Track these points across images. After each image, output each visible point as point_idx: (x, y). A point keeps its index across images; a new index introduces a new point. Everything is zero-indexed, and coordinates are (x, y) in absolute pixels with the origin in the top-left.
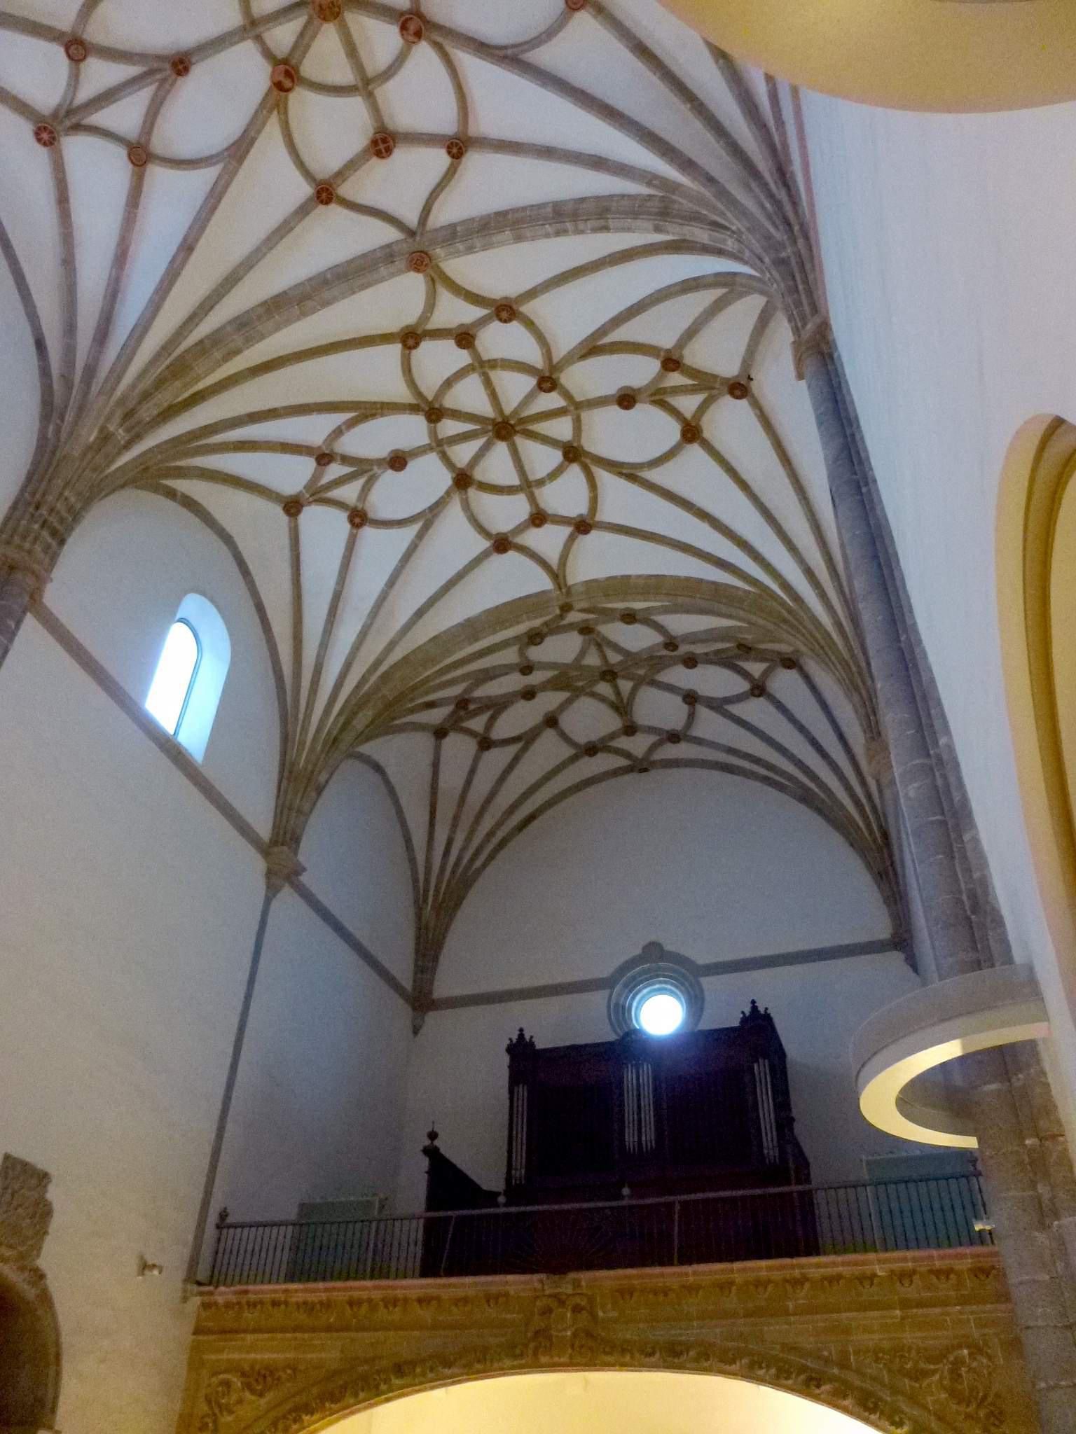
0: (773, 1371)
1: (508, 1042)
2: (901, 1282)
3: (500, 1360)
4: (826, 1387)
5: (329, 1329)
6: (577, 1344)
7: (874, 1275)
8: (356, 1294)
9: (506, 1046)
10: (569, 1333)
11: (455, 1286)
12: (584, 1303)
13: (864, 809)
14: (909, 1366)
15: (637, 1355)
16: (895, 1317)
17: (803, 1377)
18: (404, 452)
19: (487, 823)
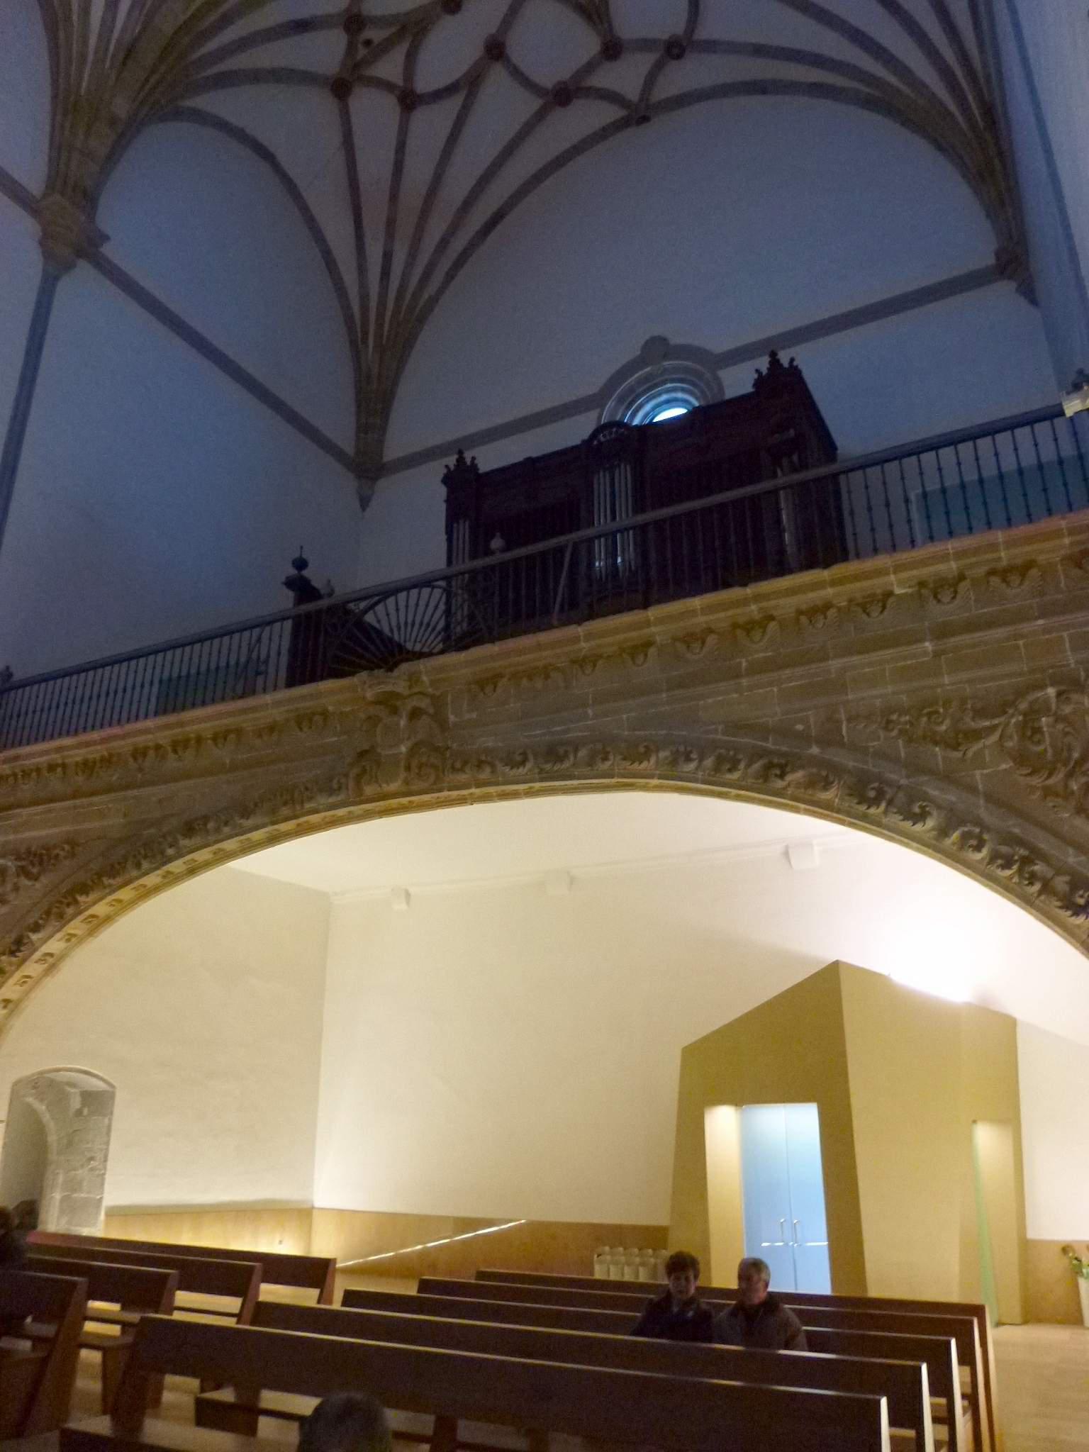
0: (709, 762)
1: (445, 471)
2: (935, 597)
3: (310, 799)
4: (798, 776)
5: (110, 789)
6: (414, 763)
7: (890, 594)
8: (141, 740)
9: (441, 476)
10: (403, 749)
11: (254, 709)
12: (424, 703)
13: (965, 99)
14: (943, 728)
15: (500, 767)
16: (925, 653)
17: (757, 766)
18: (492, 36)
19: (436, 229)
